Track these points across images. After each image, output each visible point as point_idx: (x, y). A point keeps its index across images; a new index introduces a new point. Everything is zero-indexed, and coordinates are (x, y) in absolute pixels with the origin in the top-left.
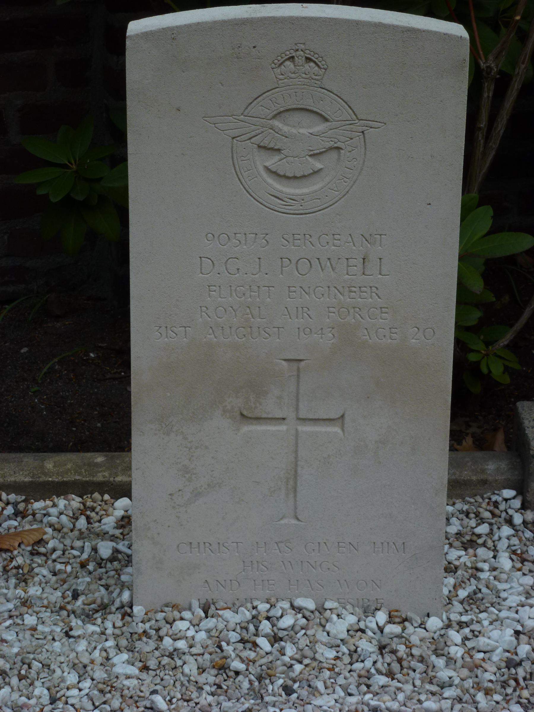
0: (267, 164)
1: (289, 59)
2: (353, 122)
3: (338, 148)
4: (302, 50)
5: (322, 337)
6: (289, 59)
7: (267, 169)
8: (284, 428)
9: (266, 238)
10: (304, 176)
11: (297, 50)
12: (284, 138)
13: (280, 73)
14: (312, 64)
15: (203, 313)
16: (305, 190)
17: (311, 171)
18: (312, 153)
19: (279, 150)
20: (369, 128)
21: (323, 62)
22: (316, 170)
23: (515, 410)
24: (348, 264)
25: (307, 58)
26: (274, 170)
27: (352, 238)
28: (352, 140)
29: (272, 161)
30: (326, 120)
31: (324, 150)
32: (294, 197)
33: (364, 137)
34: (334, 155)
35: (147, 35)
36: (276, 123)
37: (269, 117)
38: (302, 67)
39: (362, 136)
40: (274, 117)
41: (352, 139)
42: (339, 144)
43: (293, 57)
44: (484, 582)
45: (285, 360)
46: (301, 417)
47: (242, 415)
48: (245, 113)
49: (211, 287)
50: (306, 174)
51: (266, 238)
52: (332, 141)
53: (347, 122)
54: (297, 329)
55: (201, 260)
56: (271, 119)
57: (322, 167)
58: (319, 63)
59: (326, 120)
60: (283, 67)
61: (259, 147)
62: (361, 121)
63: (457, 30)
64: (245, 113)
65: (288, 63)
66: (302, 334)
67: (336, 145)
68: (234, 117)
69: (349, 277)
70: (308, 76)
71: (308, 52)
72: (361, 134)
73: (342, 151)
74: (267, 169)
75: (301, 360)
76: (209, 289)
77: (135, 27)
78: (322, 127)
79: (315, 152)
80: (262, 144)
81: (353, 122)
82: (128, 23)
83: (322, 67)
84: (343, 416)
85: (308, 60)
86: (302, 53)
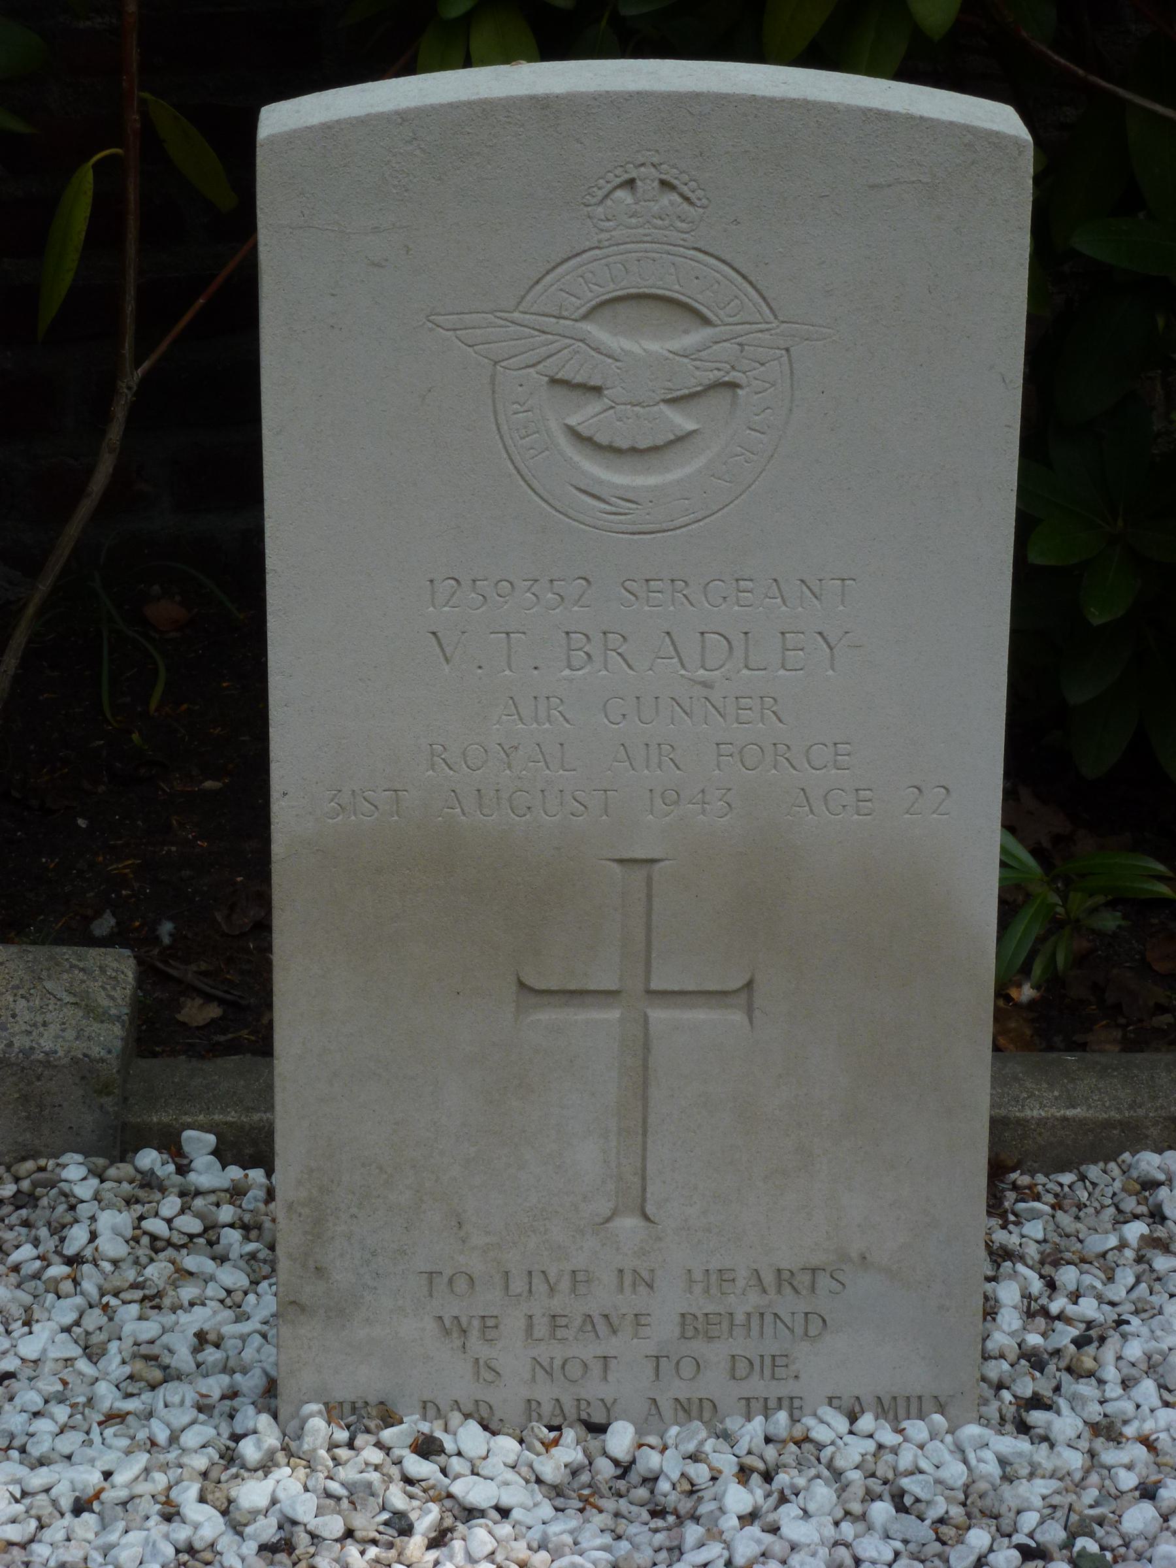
0: (572, 421)
1: (621, 186)
2: (768, 326)
3: (733, 386)
4: (654, 166)
5: (704, 812)
6: (621, 186)
7: (575, 434)
8: (614, 1014)
9: (533, 590)
10: (655, 449)
12: (610, 361)
13: (603, 217)
15: (436, 758)
16: (652, 480)
19: (597, 390)
20: (537, 333)
22: (680, 433)
24: (569, 644)
25: (664, 183)
26: (586, 433)
27: (779, 589)
29: (586, 415)
30: (706, 321)
31: (699, 388)
32: (630, 496)
33: (789, 356)
34: (721, 399)
35: (292, 138)
37: (576, 315)
38: (652, 203)
39: (785, 359)
40: (585, 317)
42: (734, 376)
45: (621, 861)
46: (654, 986)
47: (522, 985)
51: (533, 590)
52: (719, 370)
54: (649, 793)
55: (606, 638)
57: (691, 426)
59: (706, 321)
60: (609, 202)
61: (554, 381)
62: (785, 325)
63: (1002, 119)
64: (521, 309)
65: (620, 194)
66: (658, 801)
68: (498, 314)
69: (788, 673)
70: (667, 223)
73: (740, 392)
74: (575, 434)
75: (653, 861)
77: (278, 119)
78: (696, 337)
80: (559, 376)
81: (768, 326)
82: (259, 111)
83: (698, 203)
84: (749, 985)
86: (653, 170)
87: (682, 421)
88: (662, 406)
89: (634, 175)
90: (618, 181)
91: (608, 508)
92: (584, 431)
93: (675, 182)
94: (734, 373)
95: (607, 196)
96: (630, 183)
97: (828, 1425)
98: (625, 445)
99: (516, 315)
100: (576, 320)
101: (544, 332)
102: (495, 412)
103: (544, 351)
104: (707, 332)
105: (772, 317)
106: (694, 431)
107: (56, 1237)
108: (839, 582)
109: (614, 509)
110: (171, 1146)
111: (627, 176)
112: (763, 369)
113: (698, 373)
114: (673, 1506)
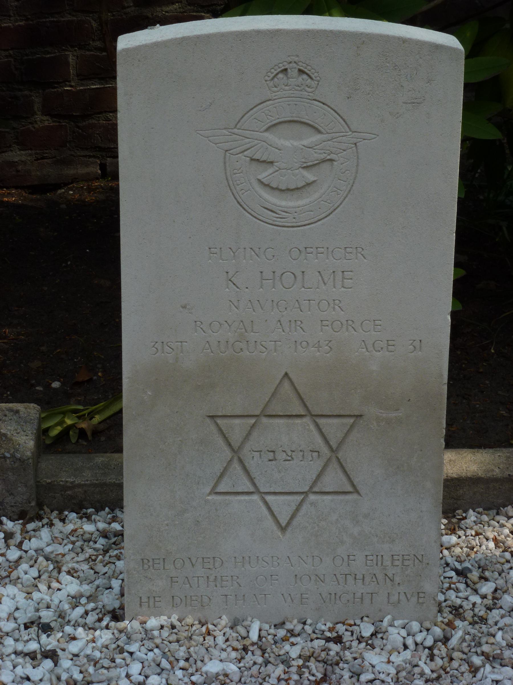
0: (260, 177)
3: (331, 160)
4: (295, 62)
11: (291, 62)
14: (305, 77)
18: (305, 165)
19: (272, 163)
29: (265, 174)
36: (266, 134)
37: (262, 130)
40: (267, 130)
43: (286, 70)
48: (238, 127)
50: (299, 186)
52: (325, 153)
59: (319, 132)
67: (329, 157)
73: (335, 163)
77: (125, 42)
85: (301, 72)
87: (310, 176)
88: (300, 169)
90: (279, 70)
91: (277, 216)
92: (264, 180)
93: (306, 70)
98: (284, 188)
99: (236, 131)
103: (248, 146)
104: (319, 137)
105: (348, 130)
106: (314, 182)
108: (274, 342)
111: (283, 68)
112: (345, 152)
113: (315, 155)
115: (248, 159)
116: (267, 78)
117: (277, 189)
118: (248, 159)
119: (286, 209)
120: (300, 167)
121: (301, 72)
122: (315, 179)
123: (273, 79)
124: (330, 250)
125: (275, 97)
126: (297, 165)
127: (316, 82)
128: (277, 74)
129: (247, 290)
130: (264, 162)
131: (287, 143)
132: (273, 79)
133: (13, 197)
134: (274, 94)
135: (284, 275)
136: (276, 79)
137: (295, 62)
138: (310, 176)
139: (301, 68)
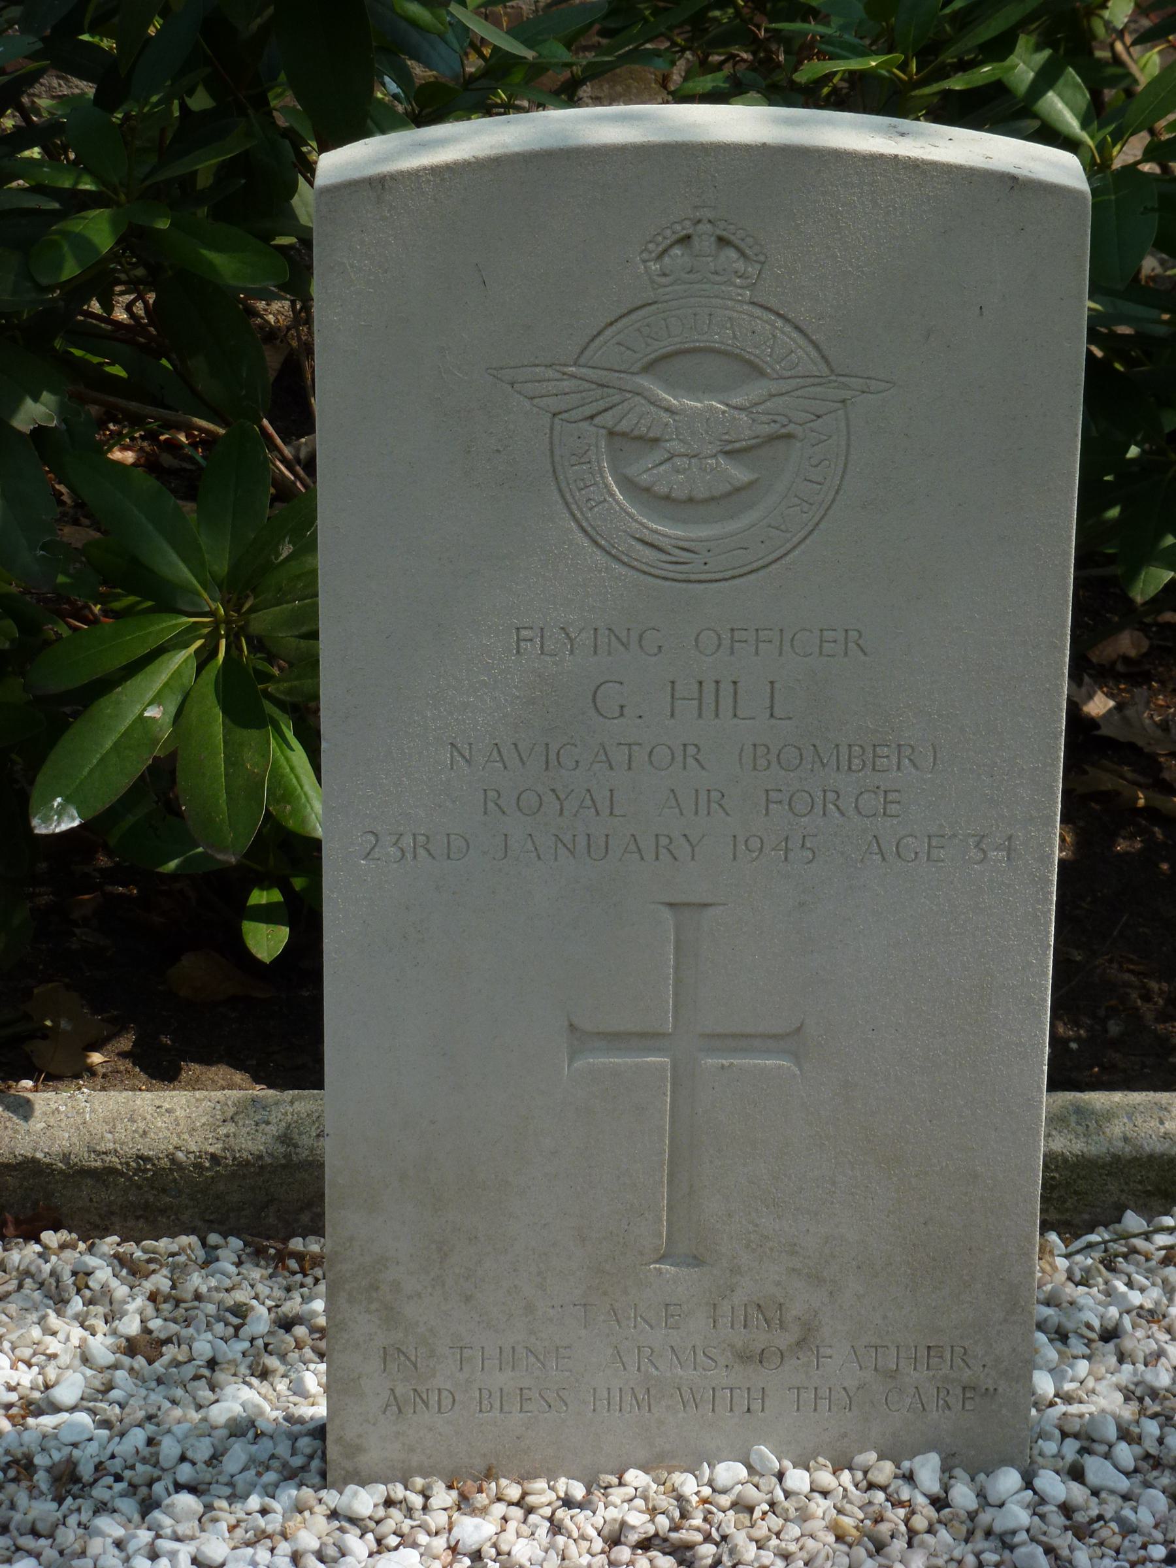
3: (789, 436)
4: (710, 221)
11: (699, 221)
14: (733, 254)
17: (728, 487)
18: (729, 447)
19: (656, 441)
20: (594, 386)
21: (750, 240)
22: (737, 484)
23: (1095, 693)
28: (820, 420)
30: (762, 374)
35: (376, 187)
36: (645, 382)
37: (635, 369)
41: (818, 417)
42: (791, 428)
43: (689, 237)
44: (1137, 1491)
48: (582, 361)
49: (825, 633)
50: (716, 494)
52: (775, 422)
53: (812, 380)
56: (637, 374)
58: (748, 251)
65: (677, 251)
67: (784, 431)
71: (722, 224)
72: (839, 405)
76: (821, 636)
77: (336, 164)
78: (756, 390)
79: (737, 445)
85: (722, 241)
86: (709, 226)
87: (739, 474)
89: (690, 231)
90: (675, 237)
93: (732, 238)
94: (792, 426)
95: (665, 251)
96: (685, 240)
97: (711, 905)
100: (633, 373)
101: (603, 386)
102: (567, 504)
103: (602, 405)
107: (1128, 1412)
109: (674, 559)
110: (234, 1159)
114: (16, 1444)
115: (604, 432)
116: (645, 256)
117: (667, 498)
118: (604, 432)
119: (682, 544)
120: (721, 451)
121: (722, 241)
122: (756, 476)
123: (660, 256)
124: (788, 636)
125: (667, 297)
126: (711, 449)
127: (758, 266)
128: (671, 246)
129: (639, 721)
130: (640, 438)
131: (318, 806)
132: (660, 256)
133: (1168, 1221)
134: (661, 290)
135: (599, 694)
136: (666, 260)
137: (710, 221)
138: (739, 474)
139: (724, 234)
